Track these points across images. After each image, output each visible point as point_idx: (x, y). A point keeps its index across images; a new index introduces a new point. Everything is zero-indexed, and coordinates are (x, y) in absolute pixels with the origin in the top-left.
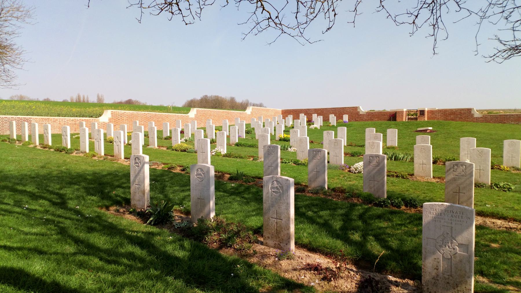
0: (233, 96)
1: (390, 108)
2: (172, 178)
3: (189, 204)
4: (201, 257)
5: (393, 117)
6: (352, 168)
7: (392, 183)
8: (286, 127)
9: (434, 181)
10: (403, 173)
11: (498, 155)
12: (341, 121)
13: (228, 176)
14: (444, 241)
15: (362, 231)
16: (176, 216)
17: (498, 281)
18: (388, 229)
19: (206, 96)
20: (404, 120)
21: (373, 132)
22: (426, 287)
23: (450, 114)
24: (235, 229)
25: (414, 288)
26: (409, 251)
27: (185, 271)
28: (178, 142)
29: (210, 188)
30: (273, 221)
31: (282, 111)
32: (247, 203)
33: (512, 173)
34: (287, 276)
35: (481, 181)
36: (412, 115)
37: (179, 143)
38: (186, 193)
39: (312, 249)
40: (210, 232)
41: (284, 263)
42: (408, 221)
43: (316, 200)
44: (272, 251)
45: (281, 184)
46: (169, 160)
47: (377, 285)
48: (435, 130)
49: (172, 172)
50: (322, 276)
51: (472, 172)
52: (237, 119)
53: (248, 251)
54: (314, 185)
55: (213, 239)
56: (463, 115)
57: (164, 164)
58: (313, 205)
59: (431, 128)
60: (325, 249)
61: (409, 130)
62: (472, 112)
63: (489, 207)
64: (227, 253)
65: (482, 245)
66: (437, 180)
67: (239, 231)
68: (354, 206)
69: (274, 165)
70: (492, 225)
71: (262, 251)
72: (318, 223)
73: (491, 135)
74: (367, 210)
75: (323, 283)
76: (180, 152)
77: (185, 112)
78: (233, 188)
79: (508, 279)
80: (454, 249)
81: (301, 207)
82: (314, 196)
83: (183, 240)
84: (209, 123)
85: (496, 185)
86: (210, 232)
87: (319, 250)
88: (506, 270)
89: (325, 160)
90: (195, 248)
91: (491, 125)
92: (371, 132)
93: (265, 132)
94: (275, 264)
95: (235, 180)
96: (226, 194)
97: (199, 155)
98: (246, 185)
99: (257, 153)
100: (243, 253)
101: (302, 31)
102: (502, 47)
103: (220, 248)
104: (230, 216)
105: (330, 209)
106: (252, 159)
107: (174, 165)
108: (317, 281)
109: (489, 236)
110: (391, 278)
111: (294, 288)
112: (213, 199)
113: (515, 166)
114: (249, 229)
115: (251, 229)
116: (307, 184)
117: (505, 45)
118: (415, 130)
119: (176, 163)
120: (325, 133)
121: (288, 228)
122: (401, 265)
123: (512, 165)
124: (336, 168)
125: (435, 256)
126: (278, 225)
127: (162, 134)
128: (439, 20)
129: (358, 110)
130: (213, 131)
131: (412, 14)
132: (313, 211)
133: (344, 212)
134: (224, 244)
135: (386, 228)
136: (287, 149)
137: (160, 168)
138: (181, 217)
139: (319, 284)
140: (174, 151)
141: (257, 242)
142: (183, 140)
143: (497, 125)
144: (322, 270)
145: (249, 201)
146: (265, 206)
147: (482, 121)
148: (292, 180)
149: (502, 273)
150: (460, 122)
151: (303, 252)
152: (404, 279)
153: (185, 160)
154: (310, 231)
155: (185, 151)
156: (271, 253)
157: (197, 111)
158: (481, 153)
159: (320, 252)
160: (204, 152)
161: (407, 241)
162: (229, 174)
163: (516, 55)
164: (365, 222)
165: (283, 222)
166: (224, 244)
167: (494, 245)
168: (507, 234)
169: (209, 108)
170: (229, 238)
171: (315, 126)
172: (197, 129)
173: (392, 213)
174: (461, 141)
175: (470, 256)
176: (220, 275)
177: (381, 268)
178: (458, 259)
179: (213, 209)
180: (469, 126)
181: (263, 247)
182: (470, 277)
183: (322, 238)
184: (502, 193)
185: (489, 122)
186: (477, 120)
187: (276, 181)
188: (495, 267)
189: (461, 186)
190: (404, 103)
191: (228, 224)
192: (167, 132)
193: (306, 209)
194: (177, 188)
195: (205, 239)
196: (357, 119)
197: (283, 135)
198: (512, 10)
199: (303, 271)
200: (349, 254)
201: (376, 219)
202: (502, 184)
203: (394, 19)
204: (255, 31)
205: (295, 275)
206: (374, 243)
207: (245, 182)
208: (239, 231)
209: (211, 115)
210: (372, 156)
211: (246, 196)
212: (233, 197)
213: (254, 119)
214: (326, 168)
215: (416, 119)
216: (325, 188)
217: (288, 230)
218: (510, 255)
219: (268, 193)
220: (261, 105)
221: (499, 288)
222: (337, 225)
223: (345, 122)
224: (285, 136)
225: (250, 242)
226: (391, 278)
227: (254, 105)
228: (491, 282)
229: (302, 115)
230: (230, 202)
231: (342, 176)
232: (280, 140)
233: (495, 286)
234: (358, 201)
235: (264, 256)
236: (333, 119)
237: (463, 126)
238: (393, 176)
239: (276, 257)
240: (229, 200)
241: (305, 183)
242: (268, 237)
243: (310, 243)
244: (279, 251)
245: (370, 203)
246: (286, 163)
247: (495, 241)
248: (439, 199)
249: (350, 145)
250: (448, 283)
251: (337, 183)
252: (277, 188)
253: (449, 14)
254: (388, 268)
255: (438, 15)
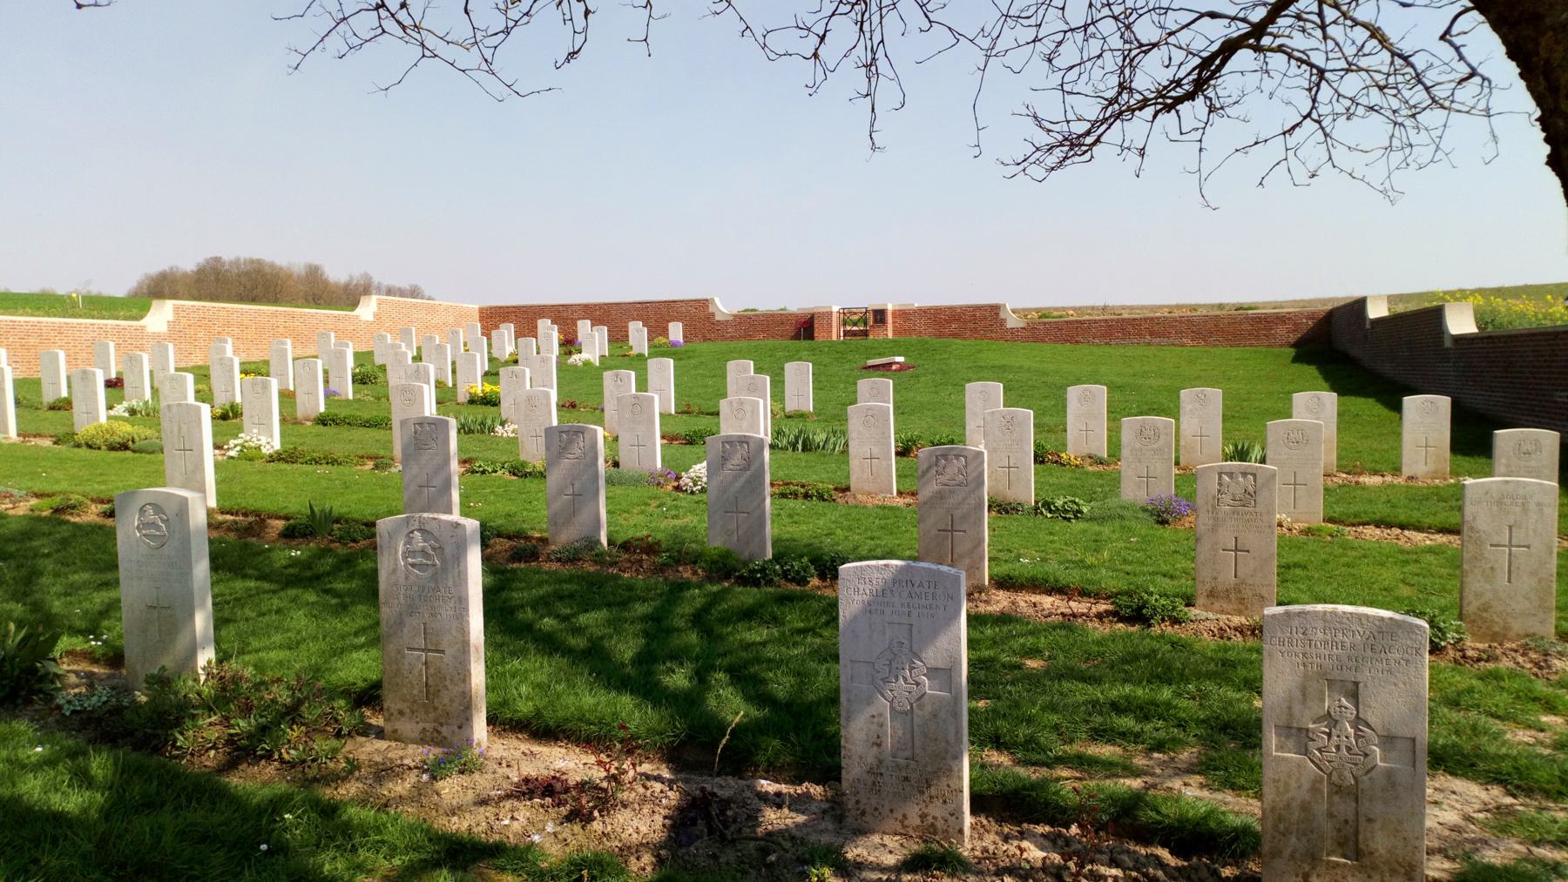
0: (316, 262)
1: (797, 303)
2: (65, 543)
3: (119, 629)
4: (150, 805)
5: (805, 327)
6: (685, 480)
7: (790, 516)
8: (491, 360)
9: (900, 502)
10: (820, 486)
11: (1051, 425)
12: (662, 340)
13: (280, 524)
14: (894, 665)
15: (697, 658)
16: (71, 669)
17: (1035, 757)
18: (769, 647)
19: (217, 259)
20: (834, 338)
21: (746, 370)
22: (853, 800)
23: (949, 322)
24: (284, 697)
25: (825, 806)
26: (819, 702)
27: (84, 857)
28: (97, 418)
29: (190, 568)
30: (415, 659)
31: (481, 311)
32: (343, 608)
33: (1087, 473)
34: (458, 825)
35: (1013, 495)
36: (855, 324)
37: (103, 419)
38: (113, 594)
39: (543, 731)
40: (194, 717)
41: (451, 788)
42: (824, 619)
43: (570, 580)
44: (413, 754)
45: (436, 540)
46: (57, 481)
47: (723, 812)
48: (913, 363)
49: (68, 522)
50: (564, 810)
51: (981, 474)
52: (325, 336)
53: (331, 765)
54: (566, 537)
55: (201, 742)
56: (980, 322)
57: (37, 496)
58: (561, 598)
59: (901, 359)
60: (584, 727)
61: (847, 366)
62: (1002, 315)
63: (1026, 564)
64: (255, 782)
65: (1004, 666)
66: (908, 500)
67: (300, 702)
68: (681, 590)
69: (437, 482)
70: (1031, 611)
71: (378, 759)
72: (568, 651)
73: (1045, 374)
74: (715, 599)
75: (567, 831)
76: (104, 453)
77: (135, 312)
78: (295, 562)
79: (1060, 749)
80: (918, 684)
81: (522, 606)
82: (567, 570)
83: (85, 754)
84: (223, 350)
85: (1047, 505)
86: (194, 717)
87: (564, 731)
88: (1056, 727)
89: (596, 459)
90: (126, 773)
91: (1047, 348)
92: (741, 371)
93: (418, 379)
94: (418, 793)
95: (304, 536)
96: (266, 586)
97: (172, 460)
98: (342, 550)
99: (388, 444)
100: (311, 773)
101: (488, 54)
102: (1044, 139)
103: (231, 765)
104: (275, 655)
105: (609, 605)
106: (370, 464)
107: (75, 498)
108: (550, 828)
109: (1022, 641)
110: (767, 786)
111: (474, 861)
112: (203, 605)
113: (1093, 452)
114: (332, 693)
115: (346, 693)
116: (545, 535)
117: (1049, 131)
118: (862, 364)
119: (88, 489)
120: (607, 375)
121: (465, 676)
122: (793, 745)
123: (1086, 451)
124: (636, 481)
125: (872, 710)
126: (432, 671)
127: (39, 392)
128: (880, 54)
129: (711, 310)
130: (232, 378)
131: (809, 29)
132: (558, 616)
133: (650, 610)
134: (241, 752)
135: (764, 644)
136: (492, 430)
137: (22, 509)
138: (90, 675)
139: (555, 834)
140: (84, 451)
141: (365, 730)
142: (120, 410)
143: (1059, 346)
144: (567, 790)
145: (347, 600)
146: (386, 613)
147: (1026, 339)
148: (472, 525)
149: (1045, 737)
150: (973, 342)
151: (515, 743)
152: (800, 784)
153: (116, 476)
154: (541, 677)
155: (124, 447)
156: (406, 762)
157: (176, 309)
158: (1010, 423)
159: (568, 738)
160: (191, 448)
161: (817, 673)
162: (287, 518)
163: (1076, 159)
164: (708, 633)
165: (447, 658)
166: (241, 752)
167: (1033, 664)
168: (1063, 633)
169: (224, 301)
170: (264, 729)
171: (585, 356)
172: (177, 369)
173: (784, 599)
174: (967, 393)
175: (956, 700)
176: (220, 853)
177: (740, 761)
178: (929, 708)
179: (205, 636)
180: (994, 353)
181: (382, 745)
182: (958, 757)
183: (576, 694)
184: (1059, 525)
185: (1043, 341)
186: (1014, 335)
187: (420, 530)
188: (1029, 720)
189: (958, 513)
190: (832, 292)
191: (263, 683)
192: (57, 384)
193: (534, 608)
194: (86, 576)
195: (175, 740)
196: (703, 336)
197: (479, 388)
198: (1059, 37)
199: (508, 804)
200: (651, 731)
201: (739, 620)
202: (1059, 503)
203: (761, 40)
204: (335, 43)
205: (481, 817)
206: (727, 692)
207: (340, 539)
208: (300, 702)
209: (229, 325)
210: (729, 441)
211: (339, 586)
212: (292, 592)
213: (384, 338)
214: (602, 482)
215: (865, 334)
216: (598, 542)
217: (464, 681)
218: (1066, 685)
219: (394, 571)
220: (414, 293)
221: (1034, 777)
222: (626, 649)
223: (674, 344)
224: (488, 388)
225: (338, 735)
226: (767, 786)
227: (389, 292)
228: (1018, 762)
229: (544, 325)
230: (278, 611)
231: (654, 503)
232: (472, 402)
233: (1022, 771)
234: (695, 573)
235: (385, 772)
236: (638, 334)
237: (980, 351)
238: (796, 495)
239: (425, 771)
240: (276, 602)
241: (541, 531)
242: (401, 713)
243: (538, 714)
244: (433, 753)
245: (727, 577)
246: (483, 472)
247: (1034, 652)
248: (908, 553)
249: (684, 411)
250: (906, 779)
251: (636, 526)
252: (423, 552)
253: (902, 34)
254: (761, 758)
255: (877, 39)
